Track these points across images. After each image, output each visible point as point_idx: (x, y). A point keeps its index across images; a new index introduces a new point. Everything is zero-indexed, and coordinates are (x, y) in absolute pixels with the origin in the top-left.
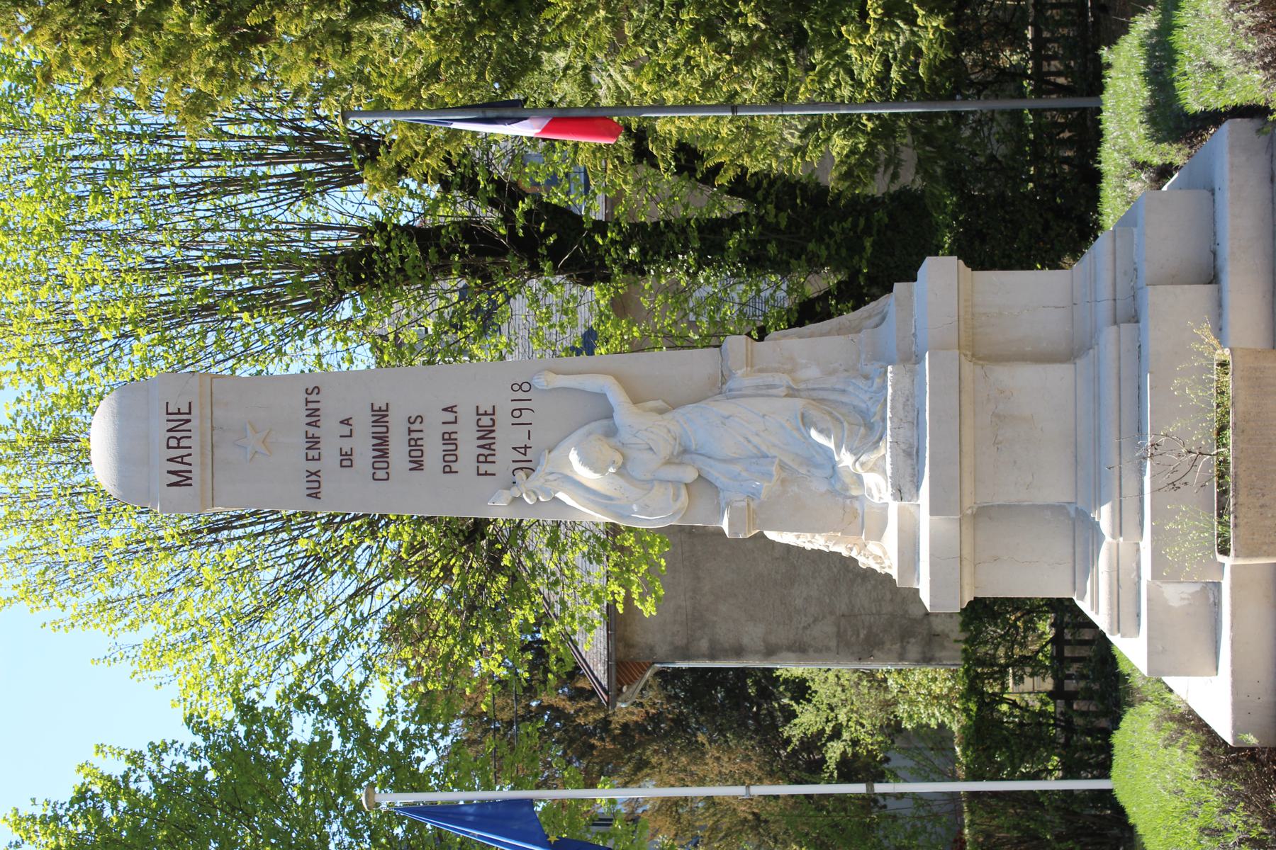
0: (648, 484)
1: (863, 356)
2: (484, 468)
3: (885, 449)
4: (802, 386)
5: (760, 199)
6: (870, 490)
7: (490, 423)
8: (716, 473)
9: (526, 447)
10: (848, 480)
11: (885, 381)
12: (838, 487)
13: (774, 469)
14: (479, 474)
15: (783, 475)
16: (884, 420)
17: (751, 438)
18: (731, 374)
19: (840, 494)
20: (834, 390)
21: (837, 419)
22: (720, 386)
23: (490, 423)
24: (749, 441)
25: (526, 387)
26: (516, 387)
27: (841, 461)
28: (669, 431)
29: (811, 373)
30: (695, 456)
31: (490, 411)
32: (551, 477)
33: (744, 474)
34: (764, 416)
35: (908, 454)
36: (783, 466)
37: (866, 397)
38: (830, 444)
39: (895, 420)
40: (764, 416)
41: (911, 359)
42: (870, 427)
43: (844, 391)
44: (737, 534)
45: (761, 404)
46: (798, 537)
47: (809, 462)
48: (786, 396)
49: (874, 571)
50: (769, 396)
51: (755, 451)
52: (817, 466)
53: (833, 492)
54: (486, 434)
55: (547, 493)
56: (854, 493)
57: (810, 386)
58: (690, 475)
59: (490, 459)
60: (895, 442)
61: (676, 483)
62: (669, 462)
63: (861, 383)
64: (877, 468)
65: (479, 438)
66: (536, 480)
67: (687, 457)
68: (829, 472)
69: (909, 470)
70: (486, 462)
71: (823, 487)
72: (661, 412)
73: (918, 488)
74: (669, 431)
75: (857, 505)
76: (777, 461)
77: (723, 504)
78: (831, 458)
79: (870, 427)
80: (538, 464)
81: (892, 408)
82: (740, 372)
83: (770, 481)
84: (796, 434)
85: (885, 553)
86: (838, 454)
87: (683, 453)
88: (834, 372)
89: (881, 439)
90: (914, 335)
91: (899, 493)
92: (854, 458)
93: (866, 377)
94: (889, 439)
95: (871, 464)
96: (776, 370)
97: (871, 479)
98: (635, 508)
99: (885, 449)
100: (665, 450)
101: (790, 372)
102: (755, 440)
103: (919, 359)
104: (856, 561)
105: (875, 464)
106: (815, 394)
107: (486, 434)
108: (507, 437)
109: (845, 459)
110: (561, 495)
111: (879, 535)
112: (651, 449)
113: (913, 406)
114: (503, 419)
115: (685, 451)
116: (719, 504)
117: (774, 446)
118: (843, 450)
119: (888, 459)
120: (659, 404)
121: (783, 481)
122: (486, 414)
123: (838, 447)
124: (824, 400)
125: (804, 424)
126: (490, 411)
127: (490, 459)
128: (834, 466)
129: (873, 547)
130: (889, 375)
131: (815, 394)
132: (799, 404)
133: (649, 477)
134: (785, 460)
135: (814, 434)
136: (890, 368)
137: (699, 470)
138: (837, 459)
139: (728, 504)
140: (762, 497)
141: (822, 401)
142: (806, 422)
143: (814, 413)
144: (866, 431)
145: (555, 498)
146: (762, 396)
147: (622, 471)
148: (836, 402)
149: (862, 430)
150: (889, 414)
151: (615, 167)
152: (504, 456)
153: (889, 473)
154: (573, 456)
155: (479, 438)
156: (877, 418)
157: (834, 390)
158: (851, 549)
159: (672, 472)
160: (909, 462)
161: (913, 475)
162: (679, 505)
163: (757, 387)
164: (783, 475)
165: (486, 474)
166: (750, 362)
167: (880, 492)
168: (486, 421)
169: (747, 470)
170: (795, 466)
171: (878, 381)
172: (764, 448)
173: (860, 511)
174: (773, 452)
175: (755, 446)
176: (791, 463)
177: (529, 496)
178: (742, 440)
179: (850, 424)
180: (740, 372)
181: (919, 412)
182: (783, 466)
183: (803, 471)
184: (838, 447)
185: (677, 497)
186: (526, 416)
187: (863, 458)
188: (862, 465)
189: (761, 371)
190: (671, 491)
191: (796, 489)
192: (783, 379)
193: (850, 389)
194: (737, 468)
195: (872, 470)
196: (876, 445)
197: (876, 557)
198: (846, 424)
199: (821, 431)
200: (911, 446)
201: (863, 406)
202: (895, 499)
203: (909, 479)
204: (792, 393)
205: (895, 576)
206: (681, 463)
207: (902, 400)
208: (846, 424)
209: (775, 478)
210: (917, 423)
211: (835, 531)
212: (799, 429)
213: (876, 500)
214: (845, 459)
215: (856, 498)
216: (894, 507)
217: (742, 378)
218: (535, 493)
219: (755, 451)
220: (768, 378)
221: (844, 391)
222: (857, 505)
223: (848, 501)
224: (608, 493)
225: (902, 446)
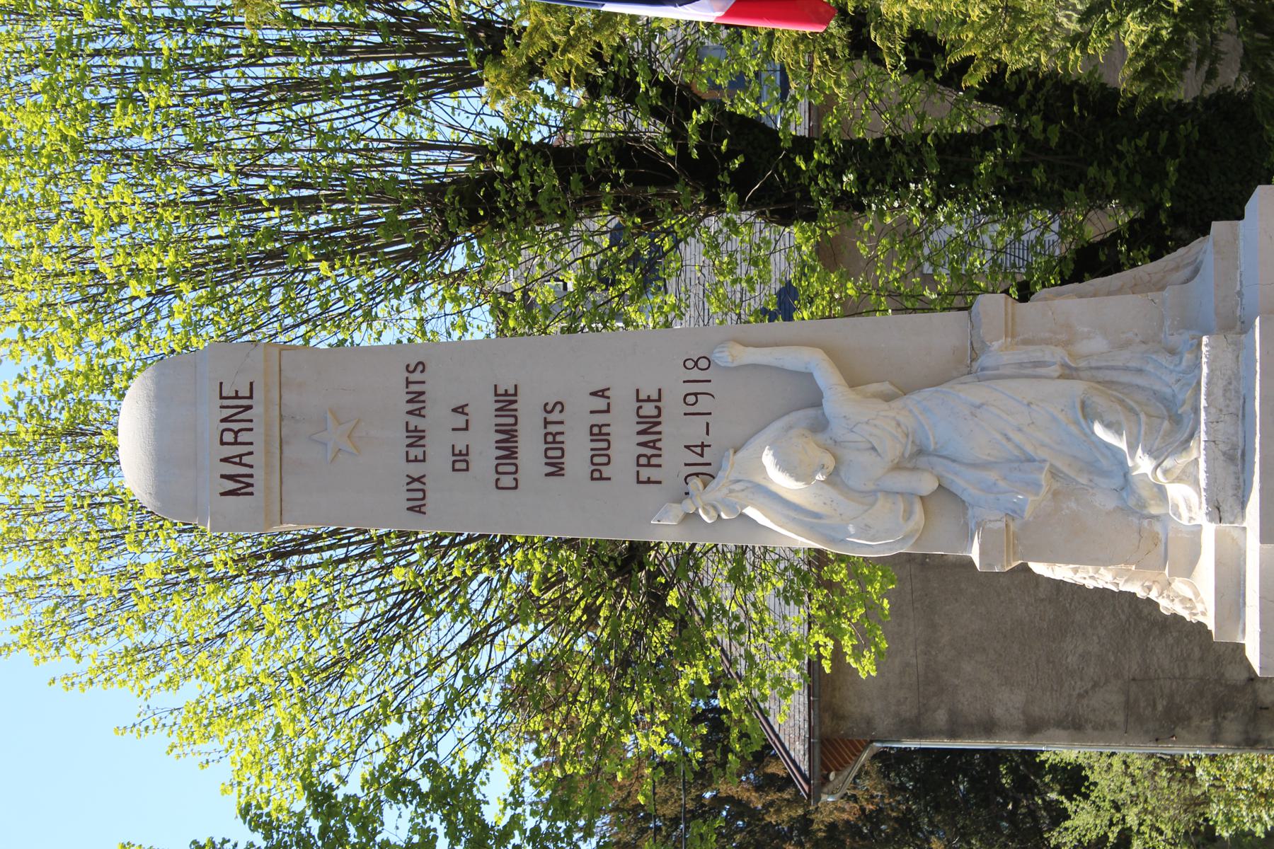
0: (868, 496)
1: (1168, 323)
2: (646, 473)
3: (1198, 451)
4: (1083, 364)
5: (1023, 106)
6: (1176, 507)
7: (655, 412)
8: (963, 483)
9: (703, 446)
10: (1145, 493)
11: (1199, 358)
12: (1132, 502)
13: (1043, 477)
14: (639, 482)
15: (1056, 485)
16: (1196, 410)
17: (1011, 435)
18: (985, 347)
19: (1134, 512)
20: (1126, 369)
21: (1131, 410)
22: (968, 363)
23: (655, 412)
24: (1009, 439)
25: (703, 364)
26: (690, 364)
27: (1136, 467)
28: (899, 424)
29: (1096, 345)
30: (935, 459)
31: (655, 396)
32: (737, 487)
33: (1002, 484)
34: (1029, 404)
35: (1230, 458)
36: (1055, 473)
37: (1171, 379)
38: (1122, 444)
39: (1213, 410)
40: (1029, 404)
41: (1234, 326)
42: (1176, 420)
43: (1140, 371)
44: (991, 566)
45: (1025, 389)
46: (1076, 571)
47: (1092, 468)
48: (1060, 377)
49: (1183, 618)
50: (1035, 377)
51: (1016, 452)
52: (1104, 474)
53: (1125, 510)
54: (650, 427)
55: (731, 507)
56: (1154, 511)
57: (1093, 364)
58: (927, 484)
59: (654, 461)
60: (1212, 442)
61: (908, 496)
62: (898, 467)
63: (1164, 359)
64: (1187, 476)
65: (639, 433)
66: (717, 491)
67: (923, 461)
68: (1118, 482)
69: (1232, 480)
70: (649, 465)
71: (1111, 503)
72: (888, 398)
73: (1243, 505)
74: (899, 424)
75: (1158, 527)
76: (1047, 466)
77: (972, 525)
78: (1123, 463)
79: (1176, 420)
80: (719, 468)
81: (1208, 395)
82: (996, 345)
83: (1037, 494)
84: (1073, 429)
85: (1197, 594)
86: (1133, 457)
87: (918, 455)
88: (1126, 345)
89: (1191, 436)
90: (1240, 294)
91: (1217, 512)
92: (1154, 463)
93: (1172, 352)
94: (1203, 437)
95: (1177, 472)
96: (1047, 342)
97: (1178, 493)
98: (851, 529)
99: (1198, 451)
100: (893, 450)
101: (1066, 344)
102: (1017, 437)
103: (1247, 327)
104: (1157, 605)
105: (1184, 471)
106: (1100, 375)
107: (650, 427)
108: (677, 432)
109: (1143, 464)
110: (751, 512)
111: (1188, 568)
112: (874, 449)
113: (1237, 392)
114: (673, 407)
115: (921, 452)
116: (966, 524)
117: (1043, 445)
118: (1140, 451)
119: (1202, 465)
120: (886, 387)
121: (1055, 494)
122: (649, 400)
123: (1132, 447)
124: (1113, 382)
125: (1085, 416)
126: (655, 396)
127: (654, 461)
128: (1126, 473)
129: (1180, 586)
130: (1204, 349)
131: (1100, 375)
132: (1077, 388)
133: (871, 486)
134: (1059, 464)
135: (1099, 430)
136: (1205, 339)
137: (939, 478)
138: (1130, 463)
139: (978, 525)
140: (1027, 515)
141: (1110, 384)
142: (1088, 413)
143: (1100, 402)
144: (1169, 425)
145: (743, 516)
146: (1027, 376)
147: (834, 479)
148: (1130, 385)
149: (1166, 424)
150: (1203, 403)
151: (825, 63)
152: (674, 457)
153: (1203, 484)
154: (768, 458)
155: (639, 433)
156: (1187, 408)
157: (1126, 369)
158: (1150, 589)
159: (902, 481)
160: (1232, 468)
161: (1237, 488)
162: (911, 525)
163: (1021, 365)
164: (1056, 485)
165: (649, 481)
166: (1011, 331)
167: (1190, 509)
168: (649, 409)
169: (1005, 479)
170: (1072, 474)
171: (1187, 357)
172: (1029, 449)
173: (1162, 536)
174: (1042, 454)
175: (1018, 447)
176: (1065, 469)
177: (706, 512)
178: (999, 437)
179: (1149, 416)
180: (996, 345)
181: (1246, 400)
182: (1055, 473)
183: (1083, 480)
184: (1132, 447)
185: (908, 515)
186: (704, 404)
187: (1168, 463)
188: (1165, 472)
189: (1026, 342)
190: (901, 506)
191: (1073, 505)
192: (1055, 354)
193: (1149, 367)
194: (992, 476)
195: (1179, 479)
196: (1185, 445)
197: (1184, 600)
198: (1143, 416)
199: (1108, 426)
200: (1234, 448)
201: (1168, 391)
202: (1211, 520)
203: (1230, 492)
204: (1069, 373)
205: (1211, 626)
206: (914, 469)
207: (1221, 383)
208: (1143, 416)
209: (1044, 490)
210: (1243, 414)
211: (1126, 563)
212: (1077, 423)
213: (1185, 522)
214: (1143, 464)
215: (1156, 517)
216: (1209, 531)
217: (999, 353)
218: (715, 508)
219: (1016, 452)
220: (1036, 353)
221: (1140, 371)
222: (1158, 527)
223: (1145, 523)
224: (815, 509)
225: (1223, 447)
